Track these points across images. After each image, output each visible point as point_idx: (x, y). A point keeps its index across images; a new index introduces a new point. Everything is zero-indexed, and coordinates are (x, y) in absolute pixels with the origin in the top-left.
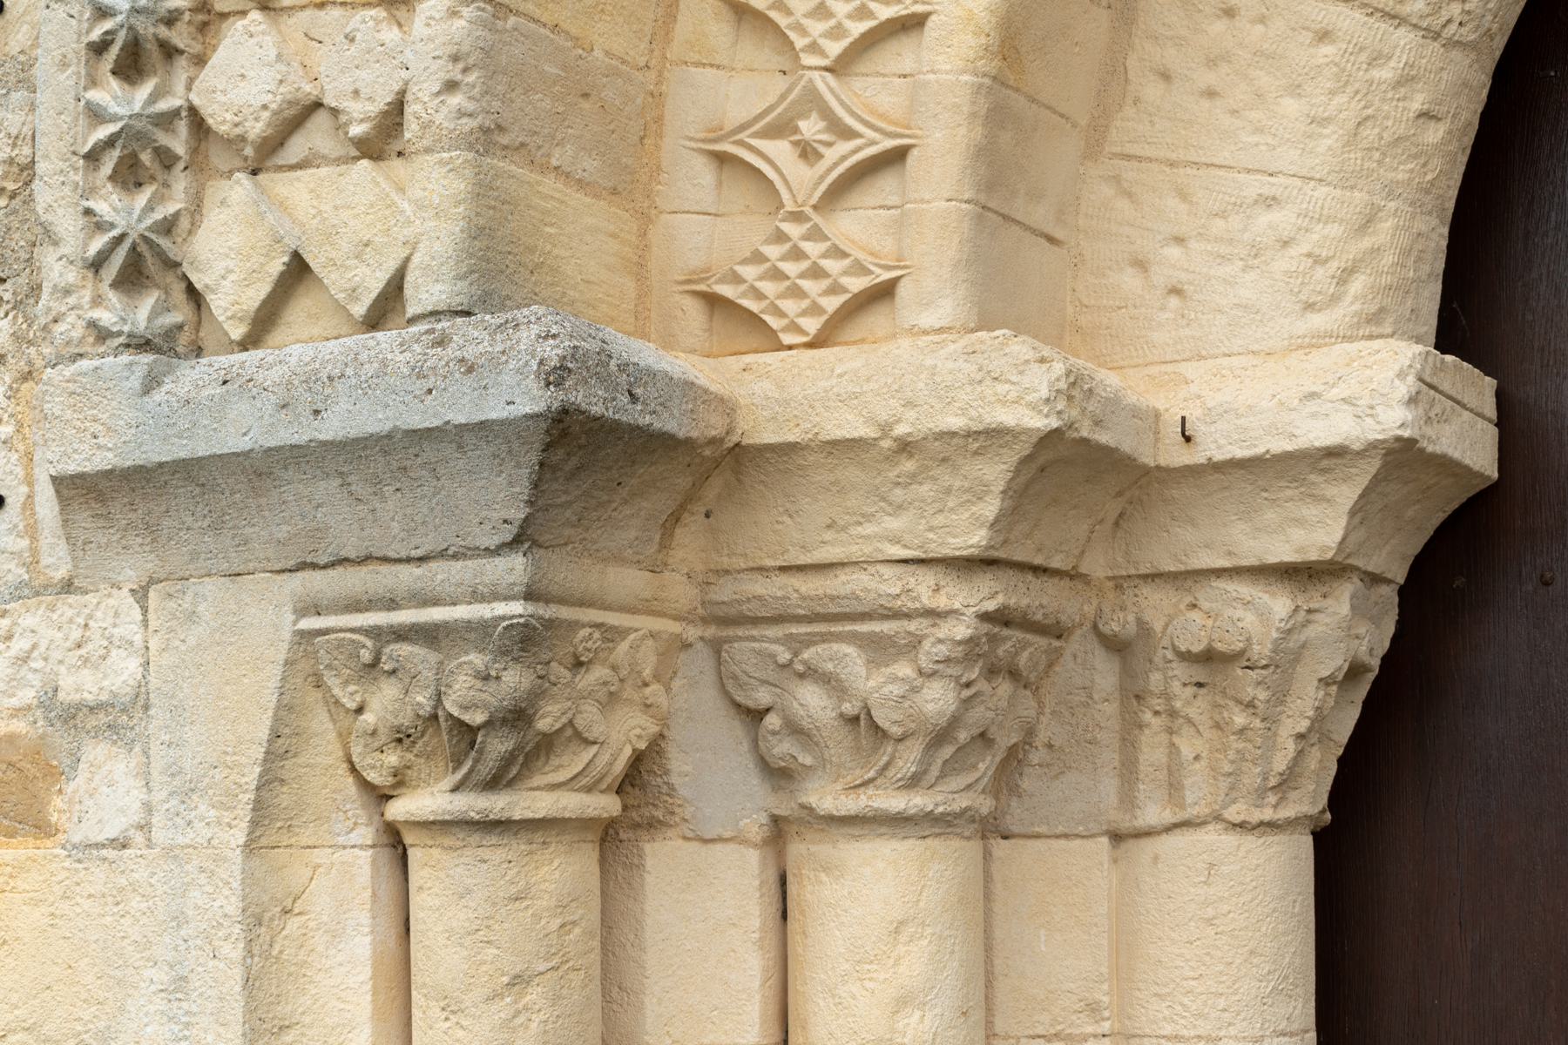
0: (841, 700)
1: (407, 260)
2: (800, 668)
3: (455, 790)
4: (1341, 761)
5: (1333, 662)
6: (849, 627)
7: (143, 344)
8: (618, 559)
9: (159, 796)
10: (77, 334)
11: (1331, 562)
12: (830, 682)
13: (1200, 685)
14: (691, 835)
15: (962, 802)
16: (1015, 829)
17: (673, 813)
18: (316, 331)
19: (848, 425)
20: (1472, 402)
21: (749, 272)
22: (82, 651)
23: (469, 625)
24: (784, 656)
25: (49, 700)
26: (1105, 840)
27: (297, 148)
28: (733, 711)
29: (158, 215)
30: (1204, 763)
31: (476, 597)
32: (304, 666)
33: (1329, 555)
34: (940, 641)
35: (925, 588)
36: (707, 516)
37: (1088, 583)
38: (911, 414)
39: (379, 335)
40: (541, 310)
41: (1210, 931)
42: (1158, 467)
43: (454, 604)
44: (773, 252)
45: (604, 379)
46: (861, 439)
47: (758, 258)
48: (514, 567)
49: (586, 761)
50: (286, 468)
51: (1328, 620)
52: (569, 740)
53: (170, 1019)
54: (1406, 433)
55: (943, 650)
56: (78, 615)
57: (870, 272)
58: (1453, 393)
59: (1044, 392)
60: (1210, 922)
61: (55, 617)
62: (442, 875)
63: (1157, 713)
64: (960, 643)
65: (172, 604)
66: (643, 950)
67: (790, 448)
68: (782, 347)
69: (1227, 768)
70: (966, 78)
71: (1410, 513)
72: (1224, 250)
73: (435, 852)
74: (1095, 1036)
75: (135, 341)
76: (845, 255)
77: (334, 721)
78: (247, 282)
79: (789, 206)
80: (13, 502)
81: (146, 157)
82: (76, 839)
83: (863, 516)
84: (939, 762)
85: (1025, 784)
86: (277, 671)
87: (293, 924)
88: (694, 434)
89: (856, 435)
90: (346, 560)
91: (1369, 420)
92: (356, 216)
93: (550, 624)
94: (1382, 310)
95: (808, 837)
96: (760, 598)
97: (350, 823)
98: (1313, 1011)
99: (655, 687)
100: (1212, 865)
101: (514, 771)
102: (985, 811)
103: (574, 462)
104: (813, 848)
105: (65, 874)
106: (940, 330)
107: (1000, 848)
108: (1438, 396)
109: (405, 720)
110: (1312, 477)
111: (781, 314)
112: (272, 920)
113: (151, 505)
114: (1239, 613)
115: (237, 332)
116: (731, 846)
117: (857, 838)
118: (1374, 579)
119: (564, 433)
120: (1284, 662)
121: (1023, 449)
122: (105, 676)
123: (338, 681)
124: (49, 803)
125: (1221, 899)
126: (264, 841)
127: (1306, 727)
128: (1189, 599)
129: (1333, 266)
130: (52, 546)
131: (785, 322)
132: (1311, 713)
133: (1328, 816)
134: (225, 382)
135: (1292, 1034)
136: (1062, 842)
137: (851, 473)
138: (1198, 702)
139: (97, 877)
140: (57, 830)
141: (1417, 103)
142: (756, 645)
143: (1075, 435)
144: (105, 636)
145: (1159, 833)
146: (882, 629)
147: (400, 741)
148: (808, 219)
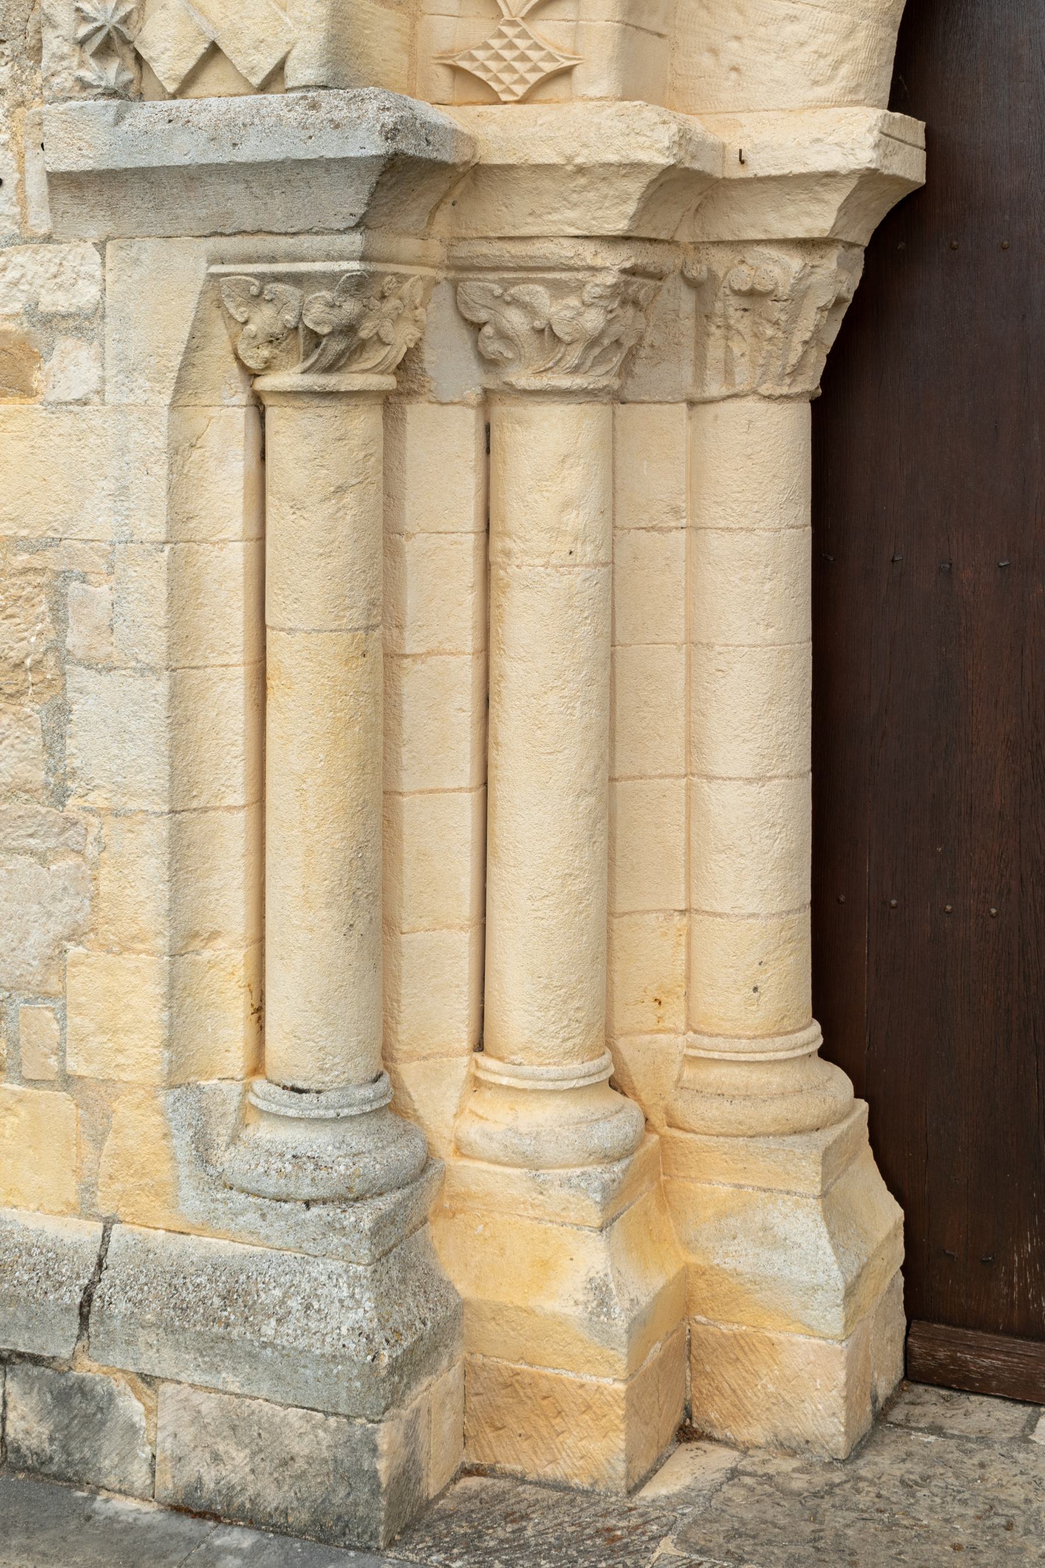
0: (533, 319)
1: (289, 52)
2: (509, 299)
4: (828, 356)
5: (826, 298)
6: (540, 275)
7: (112, 93)
8: (406, 233)
9: (110, 372)
10: (68, 84)
11: (826, 238)
13: (745, 310)
14: (434, 400)
15: (604, 382)
16: (630, 398)
17: (424, 386)
18: (222, 89)
19: (547, 155)
20: (910, 138)
21: (480, 54)
22: (58, 280)
23: (324, 275)
24: (498, 291)
25: (32, 311)
26: (684, 405)
28: (462, 323)
29: (122, 13)
30: (747, 358)
31: (329, 257)
32: (212, 295)
33: (826, 235)
34: (597, 285)
35: (588, 253)
36: (453, 204)
37: (678, 246)
38: (586, 152)
39: (269, 96)
40: (377, 91)
41: (749, 463)
42: (724, 179)
43: (314, 261)
44: (496, 43)
45: (415, 134)
46: (554, 165)
47: (487, 46)
48: (355, 241)
49: (383, 355)
50: (210, 176)
51: (823, 272)
52: (374, 343)
53: (115, 513)
54: (873, 166)
55: (598, 291)
56: (55, 257)
57: (558, 61)
58: (900, 137)
59: (667, 144)
60: (749, 457)
61: (38, 258)
62: (293, 424)
63: (719, 327)
64: (609, 287)
65: (123, 253)
66: (404, 472)
67: (511, 167)
68: (498, 102)
69: (761, 361)
71: (873, 206)
72: (765, 46)
73: (289, 410)
74: (677, 528)
75: (108, 91)
76: (541, 49)
77: (227, 328)
78: (179, 57)
79: (507, 17)
80: (9, 182)
82: (51, 399)
83: (552, 209)
84: (592, 357)
85: (637, 370)
86: (195, 298)
87: (196, 454)
88: (457, 161)
89: (551, 162)
90: (244, 232)
91: (851, 157)
92: (254, 24)
93: (372, 274)
94: (858, 85)
95: (507, 402)
96: (485, 256)
97: (232, 392)
98: (810, 513)
99: (421, 310)
100: (750, 421)
101: (343, 362)
102: (616, 387)
103: (394, 180)
104: (513, 409)
105: (42, 421)
106: (600, 99)
107: (621, 409)
108: (891, 140)
109: (277, 329)
110: (816, 188)
111: (501, 82)
112: (184, 451)
113: (114, 193)
114: (771, 267)
115: (171, 88)
116: (457, 408)
117: (539, 403)
118: (851, 245)
119: (393, 166)
120: (797, 297)
121: (653, 175)
122: (74, 297)
123: (233, 305)
124: (31, 375)
125: (756, 443)
126: (181, 402)
127: (807, 335)
128: (740, 258)
129: (830, 58)
130: (37, 213)
131: (503, 87)
132: (812, 328)
133: (820, 391)
134: (170, 121)
135: (797, 527)
136: (658, 406)
137: (547, 184)
138: (745, 320)
139: (66, 422)
140: (37, 393)
142: (481, 284)
143: (682, 166)
144: (74, 271)
145: (718, 401)
146: (561, 277)
147: (271, 342)
148: (519, 25)
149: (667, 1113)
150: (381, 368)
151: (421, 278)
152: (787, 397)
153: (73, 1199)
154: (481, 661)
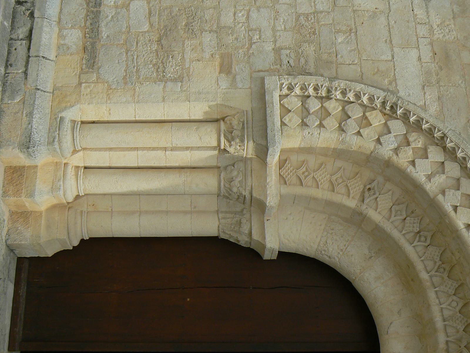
3: (224, 130)
5: (240, 238)
12: (237, 176)
20: (273, 255)
27: (304, 110)
35: (249, 188)
54: (267, 247)
55: (241, 190)
70: (310, 194)
81: (304, 91)
82: (218, 78)
102: (221, 194)
141: (308, 248)
149: (71, 207)
150: (225, 146)
151: (243, 154)
152: (219, 230)
153: (57, 85)
154: (164, 167)
